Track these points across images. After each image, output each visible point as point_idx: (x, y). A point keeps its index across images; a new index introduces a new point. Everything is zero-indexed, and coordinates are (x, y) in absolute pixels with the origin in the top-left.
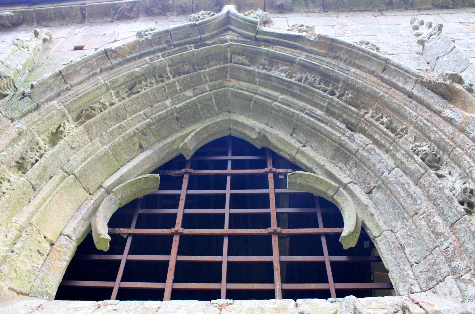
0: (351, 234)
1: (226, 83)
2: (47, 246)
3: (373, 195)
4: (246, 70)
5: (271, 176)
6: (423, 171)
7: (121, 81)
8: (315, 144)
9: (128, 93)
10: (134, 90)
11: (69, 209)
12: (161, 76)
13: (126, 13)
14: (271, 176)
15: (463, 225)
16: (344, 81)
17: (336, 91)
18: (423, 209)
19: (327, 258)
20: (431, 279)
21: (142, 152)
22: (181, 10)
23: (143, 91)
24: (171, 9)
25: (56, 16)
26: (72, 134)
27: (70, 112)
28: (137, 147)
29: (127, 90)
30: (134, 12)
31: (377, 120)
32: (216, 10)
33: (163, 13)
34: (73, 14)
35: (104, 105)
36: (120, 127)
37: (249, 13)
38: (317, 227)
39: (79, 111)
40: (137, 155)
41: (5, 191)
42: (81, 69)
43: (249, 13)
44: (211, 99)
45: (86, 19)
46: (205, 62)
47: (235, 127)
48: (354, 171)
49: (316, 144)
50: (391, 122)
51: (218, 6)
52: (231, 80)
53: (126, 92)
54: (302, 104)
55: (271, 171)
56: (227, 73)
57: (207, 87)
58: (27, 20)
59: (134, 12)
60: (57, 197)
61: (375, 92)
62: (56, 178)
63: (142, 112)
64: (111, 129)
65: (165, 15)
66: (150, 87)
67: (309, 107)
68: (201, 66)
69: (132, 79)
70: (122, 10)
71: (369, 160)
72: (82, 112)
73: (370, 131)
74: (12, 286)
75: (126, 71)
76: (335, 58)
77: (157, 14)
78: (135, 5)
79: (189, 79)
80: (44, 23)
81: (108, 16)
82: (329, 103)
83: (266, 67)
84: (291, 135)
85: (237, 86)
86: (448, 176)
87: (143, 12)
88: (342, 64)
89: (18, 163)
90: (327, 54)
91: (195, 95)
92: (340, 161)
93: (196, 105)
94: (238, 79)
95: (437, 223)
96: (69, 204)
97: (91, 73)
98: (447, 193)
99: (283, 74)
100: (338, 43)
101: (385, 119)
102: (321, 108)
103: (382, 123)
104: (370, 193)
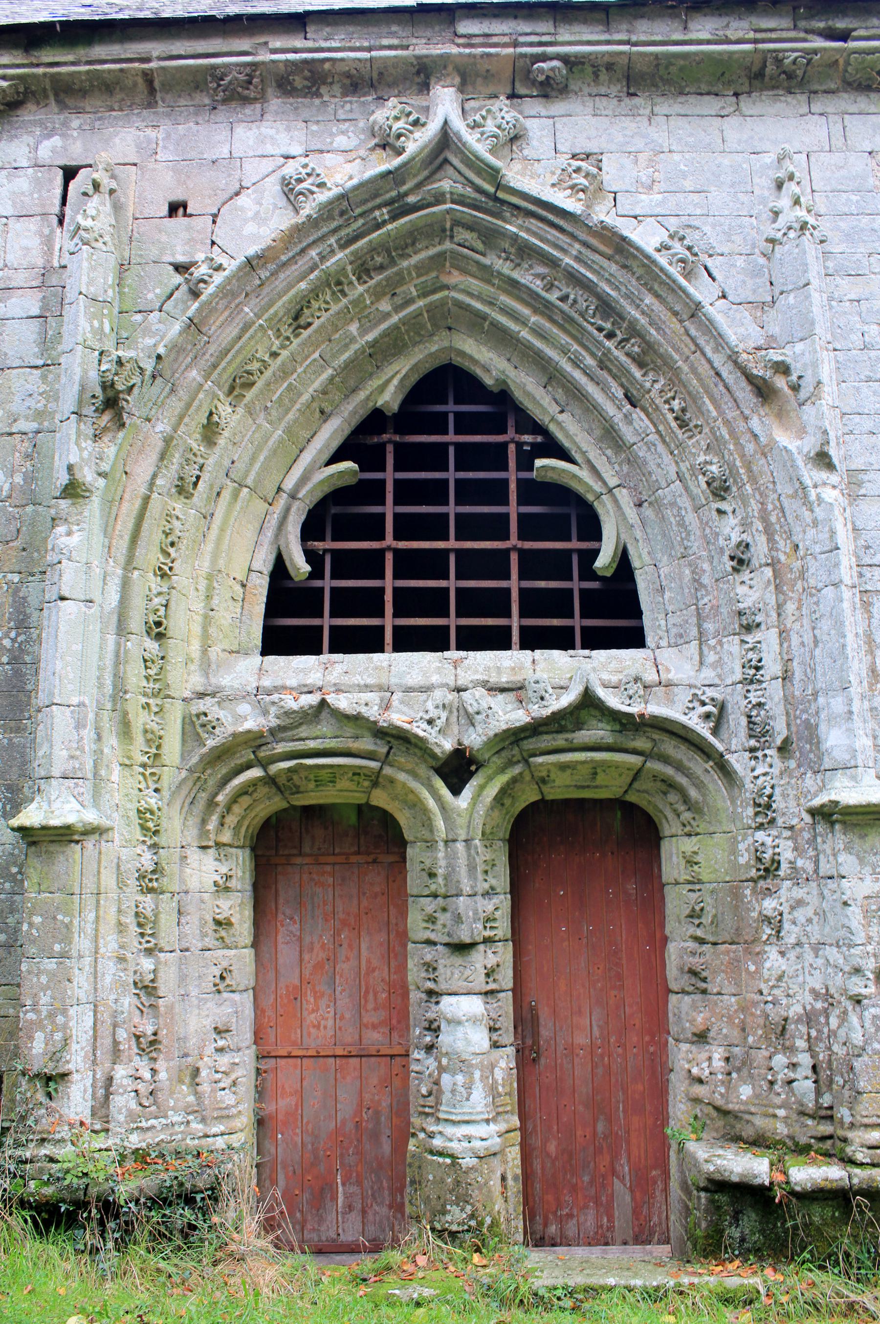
0: (606, 568)
1: (445, 280)
2: (238, 588)
3: (643, 509)
4: (477, 263)
5: (512, 448)
6: (704, 502)
7: (281, 314)
8: (578, 412)
9: (293, 327)
10: (302, 321)
11: (249, 532)
12: (339, 283)
13: (240, 90)
14: (512, 448)
15: (725, 587)
16: (630, 322)
17: (618, 332)
18: (695, 549)
19: (576, 585)
20: (681, 636)
21: (325, 421)
22: (347, 82)
23: (317, 323)
24: (330, 80)
25: (93, 86)
26: (232, 424)
27: (219, 386)
28: (317, 414)
29: (291, 321)
30: (256, 87)
31: (667, 402)
32: (418, 84)
33: (314, 89)
34: (129, 83)
35: (264, 361)
36: (290, 388)
37: (483, 118)
38: (569, 539)
39: (230, 381)
40: (320, 428)
41: (180, 534)
42: (217, 303)
43: (483, 118)
44: (421, 314)
45: (159, 96)
46: (409, 241)
47: (459, 359)
48: (625, 468)
49: (580, 412)
50: (684, 410)
51: (422, 75)
52: (452, 270)
53: (290, 325)
54: (564, 339)
55: (512, 441)
56: (445, 260)
57: (413, 289)
58: (33, 93)
59: (256, 87)
60: (236, 525)
61: (671, 357)
62: (226, 495)
63: (316, 355)
65: (318, 95)
66: (326, 310)
67: (575, 347)
68: (403, 249)
69: (297, 303)
70: (230, 83)
71: (645, 463)
72: (234, 380)
73: (654, 416)
74: (223, 647)
76: (624, 267)
77: (301, 90)
78: (254, 71)
79: (384, 283)
80: (70, 102)
81: (202, 91)
82: (604, 354)
83: (513, 257)
85: (462, 287)
86: (730, 515)
87: (274, 84)
88: (634, 282)
89: (177, 486)
90: (613, 257)
91: (397, 309)
92: (609, 447)
93: (398, 328)
94: (464, 271)
95: (704, 571)
96: (249, 526)
97: (233, 305)
98: (721, 542)
99: (538, 282)
100: (632, 246)
101: (676, 404)
102: (593, 355)
103: (672, 410)
104: (640, 505)
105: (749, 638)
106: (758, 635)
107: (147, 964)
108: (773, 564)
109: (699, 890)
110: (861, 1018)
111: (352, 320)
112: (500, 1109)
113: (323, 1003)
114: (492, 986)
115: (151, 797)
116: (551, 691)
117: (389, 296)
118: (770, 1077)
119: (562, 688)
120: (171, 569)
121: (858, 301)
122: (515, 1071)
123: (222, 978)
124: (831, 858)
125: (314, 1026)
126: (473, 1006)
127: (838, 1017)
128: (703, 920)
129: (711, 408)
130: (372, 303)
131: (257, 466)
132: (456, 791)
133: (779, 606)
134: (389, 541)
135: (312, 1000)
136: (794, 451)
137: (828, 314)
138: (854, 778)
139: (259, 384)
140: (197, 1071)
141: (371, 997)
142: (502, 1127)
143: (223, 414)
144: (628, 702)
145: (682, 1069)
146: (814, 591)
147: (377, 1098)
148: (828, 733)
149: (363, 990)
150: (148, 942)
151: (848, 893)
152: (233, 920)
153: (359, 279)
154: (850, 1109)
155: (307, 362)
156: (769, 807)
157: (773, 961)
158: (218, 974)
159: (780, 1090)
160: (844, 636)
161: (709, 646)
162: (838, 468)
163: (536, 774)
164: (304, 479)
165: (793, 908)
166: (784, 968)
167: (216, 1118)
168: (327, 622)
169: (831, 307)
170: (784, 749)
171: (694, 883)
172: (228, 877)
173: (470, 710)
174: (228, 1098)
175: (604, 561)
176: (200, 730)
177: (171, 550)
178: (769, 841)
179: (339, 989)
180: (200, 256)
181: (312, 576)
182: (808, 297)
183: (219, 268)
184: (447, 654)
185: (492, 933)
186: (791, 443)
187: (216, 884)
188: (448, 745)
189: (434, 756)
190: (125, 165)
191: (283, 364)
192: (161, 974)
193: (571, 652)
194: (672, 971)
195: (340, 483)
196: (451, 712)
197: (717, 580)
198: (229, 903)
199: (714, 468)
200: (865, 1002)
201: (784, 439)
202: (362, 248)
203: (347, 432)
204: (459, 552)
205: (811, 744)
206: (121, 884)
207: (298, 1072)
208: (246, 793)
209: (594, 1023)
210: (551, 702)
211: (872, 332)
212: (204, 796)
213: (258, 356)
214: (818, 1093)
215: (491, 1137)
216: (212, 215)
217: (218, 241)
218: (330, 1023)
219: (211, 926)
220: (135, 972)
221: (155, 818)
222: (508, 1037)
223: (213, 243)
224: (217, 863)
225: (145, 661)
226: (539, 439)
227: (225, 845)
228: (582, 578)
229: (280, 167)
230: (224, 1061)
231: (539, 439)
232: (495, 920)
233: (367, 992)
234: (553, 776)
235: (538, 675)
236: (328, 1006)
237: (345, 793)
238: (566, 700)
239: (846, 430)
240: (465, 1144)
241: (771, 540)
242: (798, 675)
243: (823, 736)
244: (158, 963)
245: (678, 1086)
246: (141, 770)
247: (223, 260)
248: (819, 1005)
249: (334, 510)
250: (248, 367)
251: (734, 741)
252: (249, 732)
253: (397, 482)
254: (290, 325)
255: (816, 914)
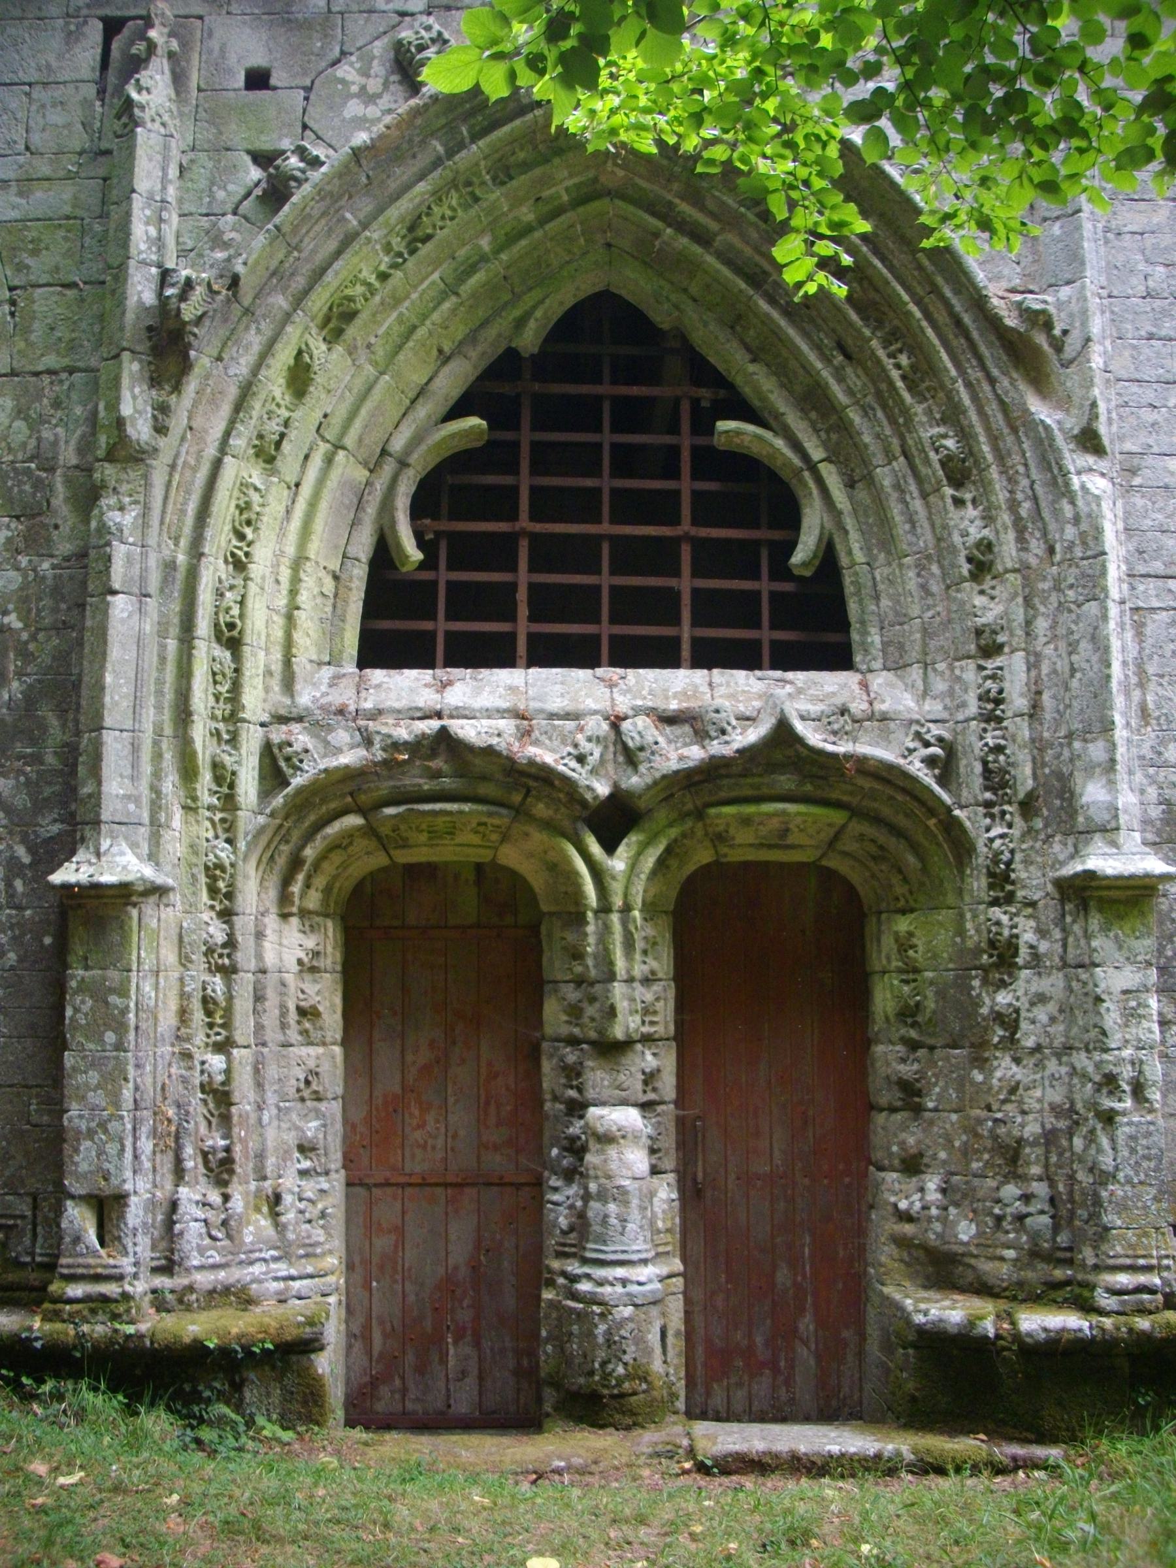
0: (804, 564)
19: (765, 586)
29: (404, 231)
35: (369, 285)
39: (325, 309)
41: (258, 509)
64: (386, 325)
75: (407, 187)
84: (732, 327)
86: (969, 505)
89: (255, 446)
105: (990, 664)
106: (999, 661)
107: (217, 1062)
108: (1023, 569)
109: (915, 980)
110: (1113, 1140)
111: (483, 231)
112: (661, 1249)
113: (430, 1118)
114: (651, 1096)
115: (222, 850)
116: (734, 722)
117: (531, 202)
118: (997, 1211)
119: (748, 719)
120: (247, 554)
121: (1142, 234)
122: (677, 1203)
123: (308, 1083)
124: (1083, 942)
125: (419, 1146)
126: (629, 1117)
127: (1085, 1138)
128: (919, 1019)
129: (949, 365)
130: (510, 210)
131: (358, 424)
132: (610, 848)
133: (1028, 623)
134: (525, 522)
135: (417, 1113)
136: (1054, 426)
137: (1102, 250)
138: (1114, 844)
139: (364, 316)
140: (277, 1198)
141: (492, 1109)
142: (664, 1270)
143: (315, 352)
144: (832, 739)
145: (887, 1203)
146: (1073, 606)
147: (498, 1237)
148: (1084, 787)
149: (482, 1100)
150: (218, 1034)
151: (1103, 985)
152: (321, 1008)
153: (494, 179)
154: (1095, 1248)
155: (424, 286)
156: (1006, 878)
157: (1005, 1068)
158: (302, 1077)
159: (1009, 1227)
160: (1109, 666)
161: (935, 670)
162: (1108, 450)
163: (710, 830)
164: (416, 440)
165: (1032, 1004)
166: (1018, 1077)
167: (302, 1257)
168: (442, 626)
169: (1107, 242)
170: (1027, 807)
171: (908, 972)
172: (316, 954)
173: (630, 744)
174: (319, 1235)
175: (802, 553)
176: (282, 764)
177: (248, 532)
178: (1005, 919)
179: (451, 1100)
180: (286, 144)
181: (422, 566)
182: (1079, 228)
183: (315, 163)
184: (599, 671)
185: (652, 1030)
186: (1049, 416)
187: (300, 962)
188: (603, 789)
189: (583, 803)
190: (186, 17)
191: (395, 289)
192: (235, 1075)
193: (758, 673)
194: (876, 1082)
195: (464, 445)
196: (606, 747)
197: (948, 587)
198: (317, 987)
199: (950, 443)
200: (1118, 1119)
201: (1041, 410)
202: (500, 139)
203: (472, 378)
204: (613, 539)
205: (1063, 799)
206: (184, 960)
207: (398, 1205)
208: (338, 846)
209: (775, 1145)
210: (734, 736)
211: (1157, 275)
212: (285, 848)
213: (361, 276)
214: (1056, 1229)
215: (650, 1281)
216: (304, 88)
217: (311, 124)
218: (440, 1142)
219: (293, 1016)
220: (202, 1072)
221: (227, 877)
222: (669, 1163)
223: (305, 127)
224: (301, 935)
225: (214, 674)
226: (722, 393)
227: (310, 912)
228: (773, 577)
229: (394, 27)
230: (310, 1188)
231: (722, 393)
232: (655, 1013)
233: (487, 1103)
234: (732, 831)
235: (719, 702)
236: (437, 1121)
237: (465, 849)
238: (752, 735)
239: (1120, 401)
240: (619, 1289)
241: (1021, 539)
242: (1048, 715)
243: (1078, 790)
244: (229, 1061)
245: (884, 1227)
246: (208, 814)
247: (318, 151)
248: (1062, 1124)
249: (450, 479)
250: (349, 292)
251: (965, 793)
252: (347, 767)
253: (696, 592)
254: (403, 237)
255: (1061, 1011)
